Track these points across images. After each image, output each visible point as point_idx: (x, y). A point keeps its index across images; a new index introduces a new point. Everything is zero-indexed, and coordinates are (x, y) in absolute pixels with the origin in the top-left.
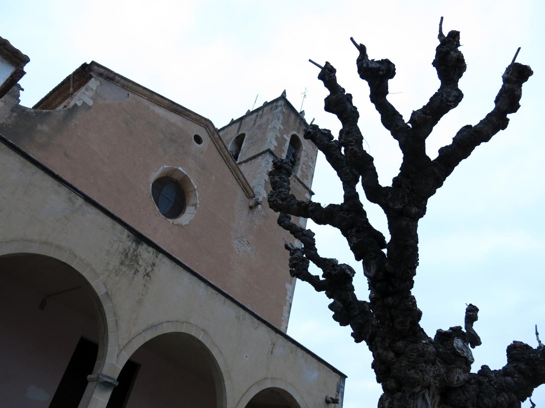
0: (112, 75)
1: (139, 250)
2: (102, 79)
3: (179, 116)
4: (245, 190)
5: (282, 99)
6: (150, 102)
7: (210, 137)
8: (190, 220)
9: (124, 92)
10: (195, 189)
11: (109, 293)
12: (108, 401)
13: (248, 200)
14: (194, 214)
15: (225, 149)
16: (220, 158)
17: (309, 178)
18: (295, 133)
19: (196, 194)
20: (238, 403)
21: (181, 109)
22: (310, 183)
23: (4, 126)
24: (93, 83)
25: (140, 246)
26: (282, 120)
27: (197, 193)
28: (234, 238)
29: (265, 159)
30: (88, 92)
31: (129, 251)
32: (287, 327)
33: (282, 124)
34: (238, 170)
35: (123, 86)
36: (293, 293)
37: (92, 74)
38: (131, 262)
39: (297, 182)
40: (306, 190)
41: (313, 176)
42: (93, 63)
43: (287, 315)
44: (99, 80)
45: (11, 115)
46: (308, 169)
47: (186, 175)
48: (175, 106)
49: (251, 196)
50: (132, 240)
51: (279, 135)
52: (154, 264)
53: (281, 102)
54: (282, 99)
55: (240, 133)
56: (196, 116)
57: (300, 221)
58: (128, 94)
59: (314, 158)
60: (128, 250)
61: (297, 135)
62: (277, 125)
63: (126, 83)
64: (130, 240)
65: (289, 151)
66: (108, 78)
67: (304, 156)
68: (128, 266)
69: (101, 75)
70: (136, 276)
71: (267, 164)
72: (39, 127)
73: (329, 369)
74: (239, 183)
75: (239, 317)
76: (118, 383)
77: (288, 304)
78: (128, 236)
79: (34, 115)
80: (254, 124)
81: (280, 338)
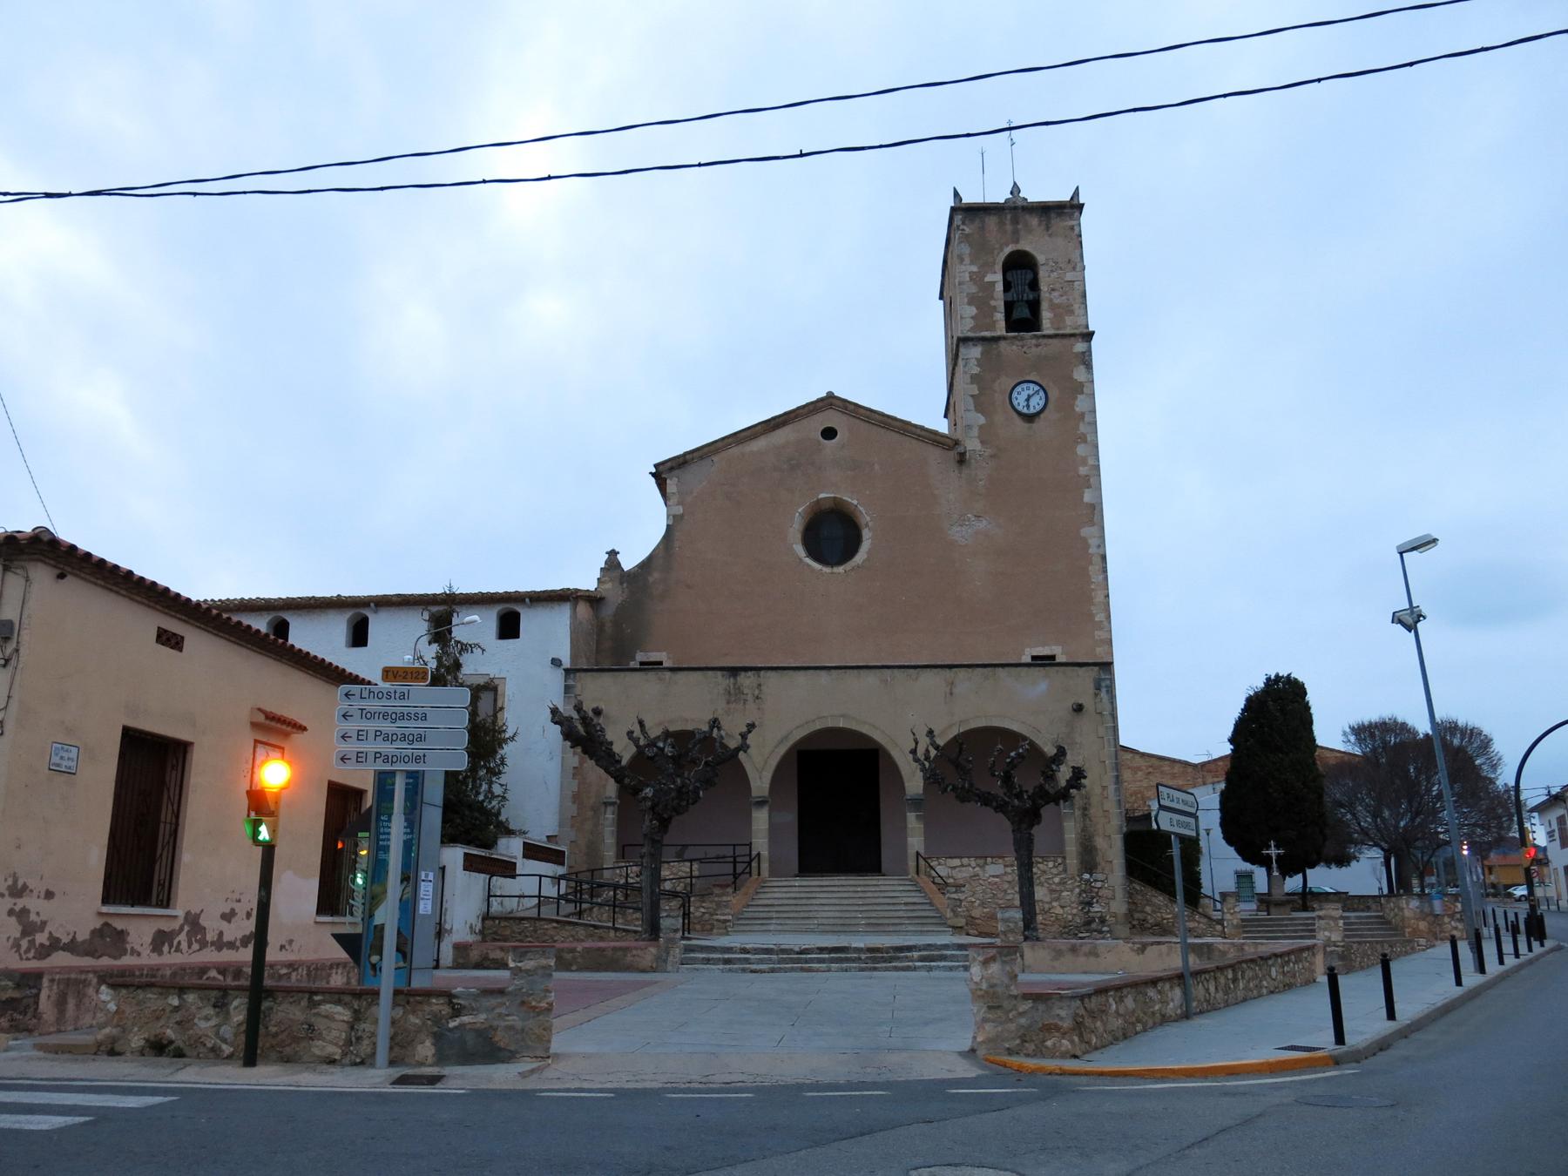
0: (681, 460)
4: (938, 443)
6: (740, 446)
11: (729, 732)
17: (1076, 306)
18: (1008, 250)
21: (781, 419)
27: (861, 508)
33: (972, 263)
35: (701, 458)
36: (1102, 537)
39: (1045, 341)
40: (1072, 339)
41: (1084, 296)
43: (1101, 577)
51: (974, 289)
52: (760, 685)
63: (700, 453)
66: (680, 465)
69: (672, 469)
78: (723, 676)
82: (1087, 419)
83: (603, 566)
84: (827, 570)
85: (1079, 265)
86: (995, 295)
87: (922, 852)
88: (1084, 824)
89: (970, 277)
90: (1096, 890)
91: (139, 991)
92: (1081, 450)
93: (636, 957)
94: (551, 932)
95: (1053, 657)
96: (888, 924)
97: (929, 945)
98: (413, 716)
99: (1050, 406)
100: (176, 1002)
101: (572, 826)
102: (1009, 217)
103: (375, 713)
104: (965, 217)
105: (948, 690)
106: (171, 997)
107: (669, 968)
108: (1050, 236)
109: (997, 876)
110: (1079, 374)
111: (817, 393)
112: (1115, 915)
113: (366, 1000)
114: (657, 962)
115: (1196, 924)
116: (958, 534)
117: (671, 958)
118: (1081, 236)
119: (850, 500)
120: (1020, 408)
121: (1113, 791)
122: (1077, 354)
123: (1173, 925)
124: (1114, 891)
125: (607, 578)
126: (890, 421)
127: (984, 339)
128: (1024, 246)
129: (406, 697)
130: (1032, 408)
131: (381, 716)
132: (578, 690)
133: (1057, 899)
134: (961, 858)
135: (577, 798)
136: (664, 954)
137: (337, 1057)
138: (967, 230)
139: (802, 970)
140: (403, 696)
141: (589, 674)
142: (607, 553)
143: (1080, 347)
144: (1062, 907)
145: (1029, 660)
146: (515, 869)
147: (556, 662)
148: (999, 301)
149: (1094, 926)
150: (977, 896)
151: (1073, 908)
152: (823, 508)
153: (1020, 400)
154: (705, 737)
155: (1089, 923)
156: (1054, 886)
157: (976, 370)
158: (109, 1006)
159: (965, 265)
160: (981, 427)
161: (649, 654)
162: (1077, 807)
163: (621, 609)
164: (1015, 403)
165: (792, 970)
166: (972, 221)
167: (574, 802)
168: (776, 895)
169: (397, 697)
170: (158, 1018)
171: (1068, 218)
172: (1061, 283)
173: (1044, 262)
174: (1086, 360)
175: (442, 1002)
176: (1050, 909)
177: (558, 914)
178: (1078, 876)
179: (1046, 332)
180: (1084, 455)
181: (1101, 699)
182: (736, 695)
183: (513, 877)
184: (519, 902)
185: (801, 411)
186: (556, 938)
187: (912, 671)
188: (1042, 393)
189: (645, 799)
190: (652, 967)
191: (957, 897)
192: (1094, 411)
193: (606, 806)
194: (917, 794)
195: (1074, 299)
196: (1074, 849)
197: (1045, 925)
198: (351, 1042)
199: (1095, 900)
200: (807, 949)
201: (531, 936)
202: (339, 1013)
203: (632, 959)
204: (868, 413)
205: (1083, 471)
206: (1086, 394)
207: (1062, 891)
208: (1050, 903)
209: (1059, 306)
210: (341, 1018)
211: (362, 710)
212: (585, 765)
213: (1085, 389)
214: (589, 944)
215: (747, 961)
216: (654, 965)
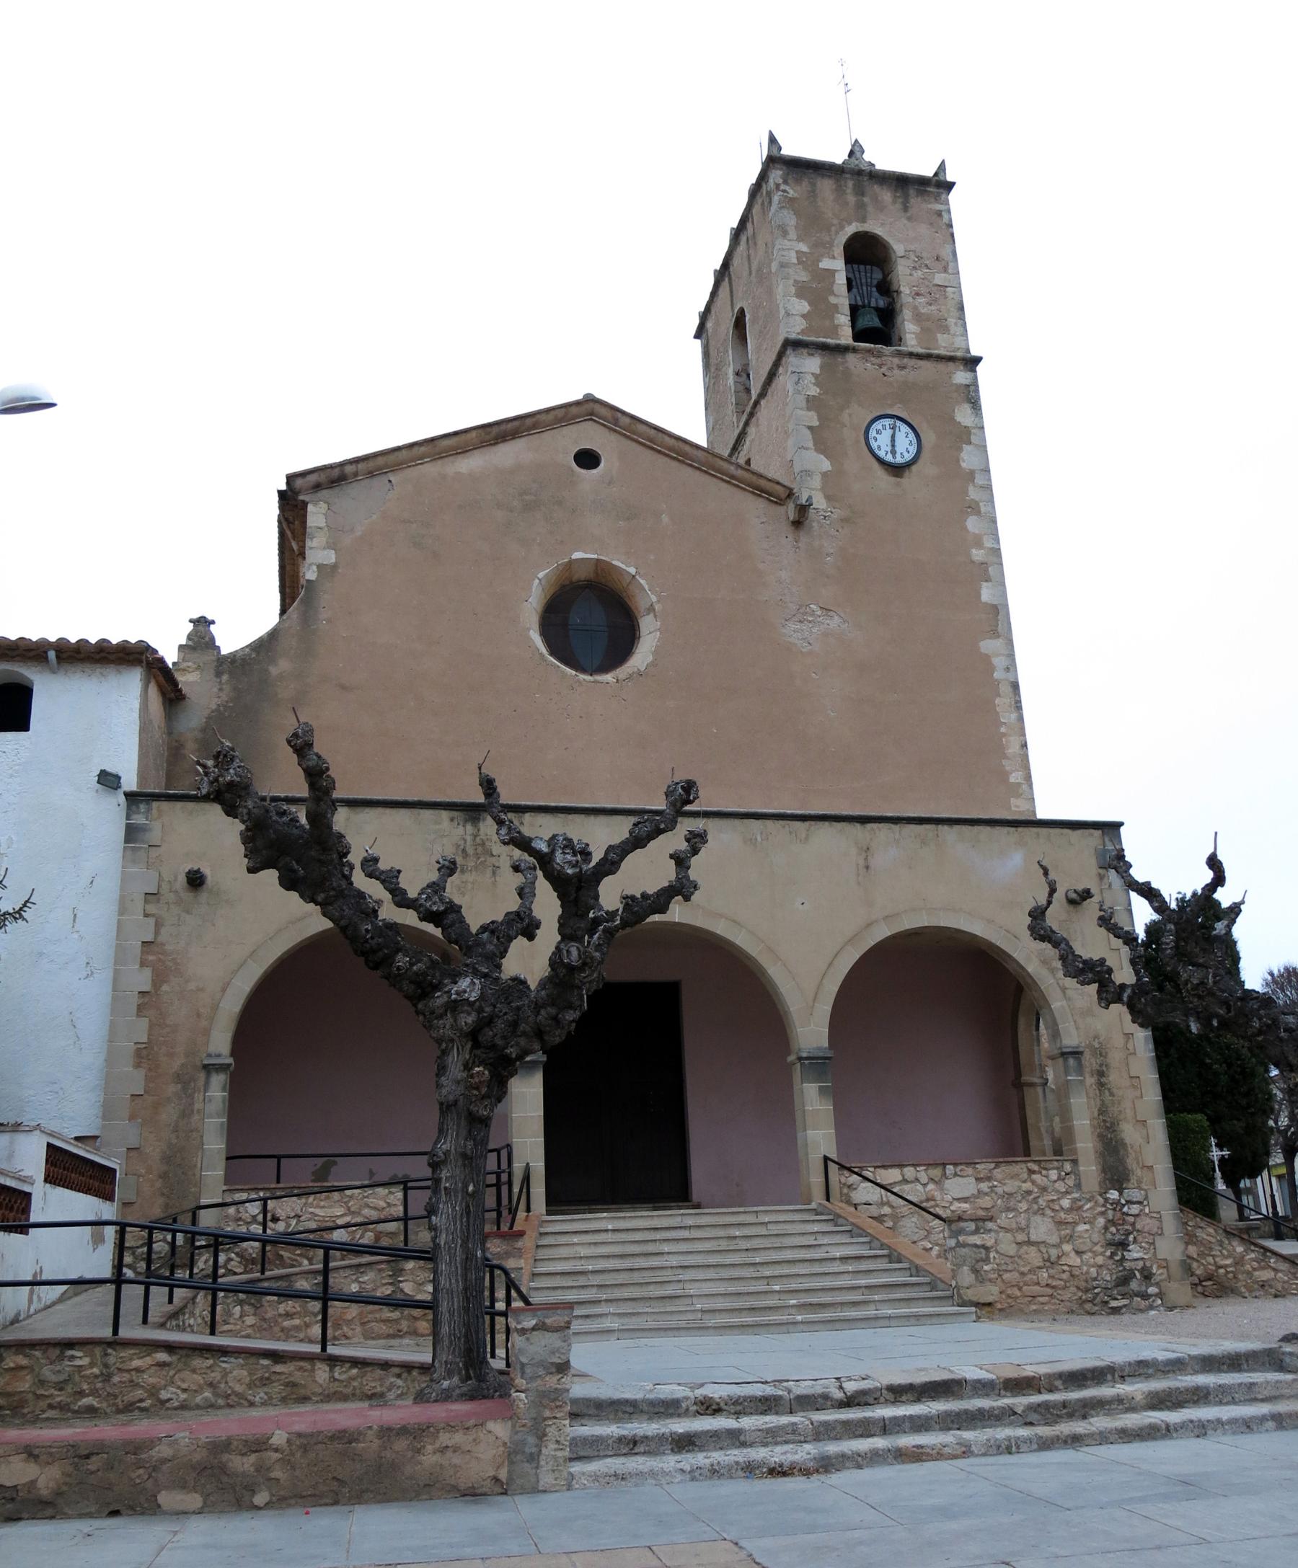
0: (336, 472)
1: (482, 832)
2: (325, 493)
3: (518, 440)
4: (762, 491)
5: (771, 165)
6: (440, 462)
7: (615, 431)
8: (653, 649)
9: (380, 482)
10: (634, 576)
12: (542, 1089)
13: (781, 509)
14: (655, 631)
15: (660, 434)
16: (663, 460)
17: (951, 321)
18: (851, 229)
19: (641, 584)
20: (816, 994)
21: (510, 426)
22: (959, 330)
23: (222, 708)
24: (316, 516)
26: (796, 227)
27: (642, 582)
28: (783, 621)
29: (790, 369)
31: (465, 843)
32: (1026, 743)
33: (800, 239)
34: (718, 460)
35: (371, 474)
36: (1011, 656)
37: (301, 498)
38: (479, 858)
39: (913, 362)
40: (951, 364)
41: (961, 308)
42: (291, 478)
43: (1014, 716)
44: (320, 500)
46: (936, 300)
47: (598, 560)
48: (495, 430)
49: (783, 496)
50: (461, 823)
51: (804, 277)
53: (776, 175)
54: (771, 165)
55: (736, 311)
56: (552, 413)
57: (964, 461)
58: (390, 481)
59: (945, 252)
60: (462, 843)
61: (861, 229)
62: (784, 253)
63: (371, 464)
64: (458, 824)
65: (865, 288)
66: (333, 482)
67: (908, 272)
68: (476, 868)
69: (317, 487)
70: (498, 879)
71: (797, 383)
73: (1057, 831)
74: (738, 486)
75: (751, 839)
76: (545, 1055)
77: (1005, 689)
78: (452, 820)
79: (253, 656)
80: (750, 273)
81: (880, 830)
82: (979, 480)
83: (184, 642)
85: (951, 265)
86: (835, 288)
87: (833, 1156)
88: (1102, 1101)
89: (798, 258)
90: (1131, 1219)
92: (972, 524)
93: (449, 1454)
94: (149, 1379)
96: (842, 1304)
97: (1141, 1363)
99: (925, 454)
101: (132, 1117)
104: (788, 174)
105: (862, 862)
107: (546, 1479)
108: (909, 219)
109: (964, 1200)
110: (963, 415)
111: (569, 393)
112: (1165, 1265)
114: (511, 1463)
115: (1273, 1274)
116: (794, 632)
117: (549, 1449)
118: (951, 226)
119: (623, 566)
120: (881, 454)
121: (1142, 1041)
122: (959, 386)
123: (1235, 1277)
124: (1160, 1219)
125: (190, 664)
126: (687, 448)
127: (824, 348)
130: (898, 455)
132: (155, 835)
133: (1070, 1238)
134: (901, 1166)
135: (144, 1055)
136: (531, 1440)
138: (791, 193)
139: (901, 1456)
141: (179, 805)
142: (191, 621)
143: (961, 377)
144: (1079, 1253)
146: (26, 1210)
147: (108, 780)
148: (842, 299)
149: (1134, 1285)
150: (933, 1238)
151: (1095, 1254)
152: (575, 578)
153: (881, 441)
155: (1124, 1280)
156: (1062, 1215)
157: (814, 391)
159: (790, 240)
160: (825, 475)
162: (1088, 1070)
163: (218, 719)
164: (874, 445)
165: (875, 1458)
166: (798, 181)
167: (137, 1065)
168: (584, 1251)
171: (933, 200)
173: (903, 254)
174: (971, 397)
176: (1059, 1257)
177: (145, 1321)
178: (1101, 1195)
181: (1110, 885)
182: (477, 855)
183: (23, 1229)
184: (31, 1293)
185: (543, 417)
186: (164, 1395)
187: (798, 824)
188: (899, 423)
189: (454, 1006)
190: (496, 1480)
191: (979, 1243)
192: (987, 470)
194: (819, 1049)
196: (1090, 1145)
197: (1053, 1287)
199: (1131, 1238)
200: (864, 1393)
201: (94, 1393)
203: (435, 1458)
204: (653, 432)
205: (978, 555)
206: (976, 445)
207: (1076, 1224)
208: (1057, 1246)
209: (928, 318)
212: (165, 988)
213: (973, 437)
214: (306, 1418)
215: (735, 1438)
216: (503, 1475)
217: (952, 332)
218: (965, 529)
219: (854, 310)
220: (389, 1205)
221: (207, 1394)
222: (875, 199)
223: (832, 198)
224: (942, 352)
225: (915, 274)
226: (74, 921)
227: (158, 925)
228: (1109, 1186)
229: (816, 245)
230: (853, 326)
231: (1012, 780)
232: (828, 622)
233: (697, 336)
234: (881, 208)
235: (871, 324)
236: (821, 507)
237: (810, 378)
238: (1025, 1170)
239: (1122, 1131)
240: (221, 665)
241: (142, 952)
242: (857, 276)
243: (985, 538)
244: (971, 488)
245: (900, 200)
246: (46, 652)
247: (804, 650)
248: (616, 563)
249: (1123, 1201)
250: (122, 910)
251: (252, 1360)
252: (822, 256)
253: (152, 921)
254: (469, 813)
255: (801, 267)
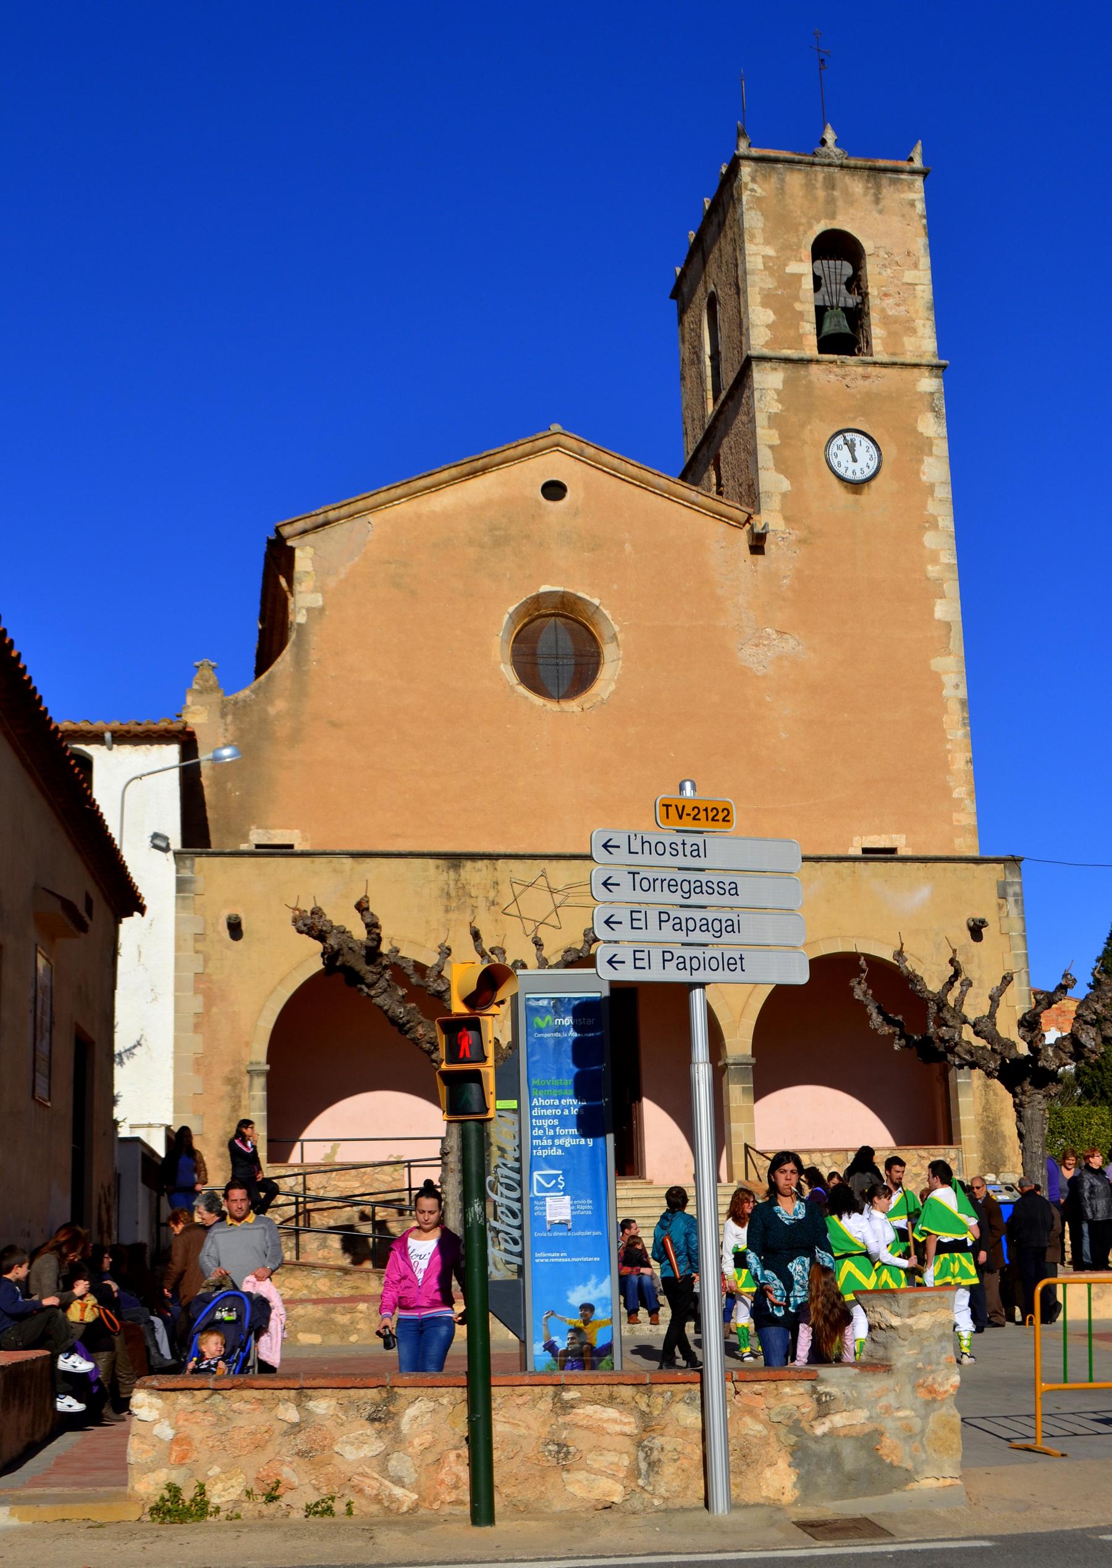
1: (462, 877)
4: (721, 516)
18: (819, 228)
25: (461, 870)
27: (606, 612)
30: (303, 584)
33: (767, 242)
40: (916, 371)
44: (307, 545)
45: (226, 724)
50: (445, 870)
57: (924, 474)
61: (830, 227)
65: (833, 286)
68: (458, 908)
72: (272, 711)
78: (437, 867)
84: (552, 706)
88: (987, 1100)
89: (764, 264)
91: (217, 1398)
95: (893, 851)
98: (715, 887)
100: (291, 1414)
102: (820, 177)
103: (654, 881)
106: (281, 1407)
108: (880, 212)
113: (661, 1394)
116: (750, 657)
122: (922, 395)
127: (787, 360)
128: (843, 223)
129: (702, 853)
131: (665, 884)
132: (199, 886)
135: (201, 1065)
137: (617, 1499)
140: (696, 852)
145: (859, 853)
148: (807, 303)
153: (841, 457)
154: (580, 957)
158: (157, 1430)
160: (784, 495)
161: (273, 832)
166: (765, 177)
169: (688, 853)
170: (259, 1447)
171: (906, 188)
172: (897, 286)
173: (872, 252)
175: (802, 1390)
179: (877, 358)
180: (934, 547)
182: (459, 897)
193: (251, 1077)
194: (744, 1056)
195: (917, 311)
198: (639, 1470)
202: (615, 1421)
206: (937, 456)
209: (896, 320)
210: (618, 1428)
211: (634, 874)
212: (214, 1010)
213: (934, 448)
217: (920, 334)
218: (921, 544)
219: (821, 312)
220: (394, 1180)
221: (305, 1292)
222: (846, 192)
223: (801, 194)
224: (909, 359)
225: (884, 273)
226: (140, 956)
227: (206, 960)
228: (988, 1170)
229: (784, 248)
230: (818, 334)
231: (955, 795)
232: (783, 645)
233: (672, 297)
234: (850, 201)
235: (837, 330)
236: (780, 529)
237: (772, 395)
238: (916, 1156)
239: (1002, 1125)
240: (225, 707)
241: (195, 981)
242: (827, 273)
243: (942, 553)
244: (930, 501)
245: (872, 191)
246: (103, 733)
247: (759, 674)
248: (580, 594)
249: (998, 1182)
250: (178, 948)
251: (332, 1272)
252: (789, 259)
253: (201, 957)
254: (452, 861)
255: (767, 273)
